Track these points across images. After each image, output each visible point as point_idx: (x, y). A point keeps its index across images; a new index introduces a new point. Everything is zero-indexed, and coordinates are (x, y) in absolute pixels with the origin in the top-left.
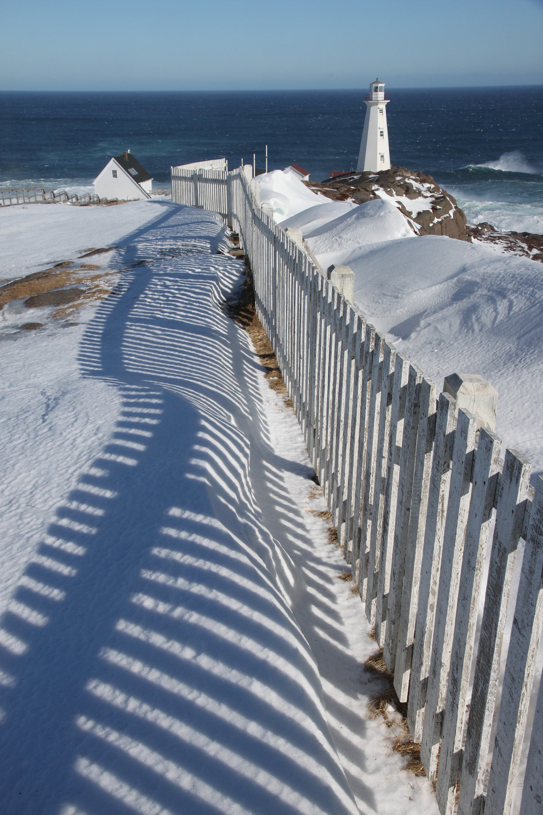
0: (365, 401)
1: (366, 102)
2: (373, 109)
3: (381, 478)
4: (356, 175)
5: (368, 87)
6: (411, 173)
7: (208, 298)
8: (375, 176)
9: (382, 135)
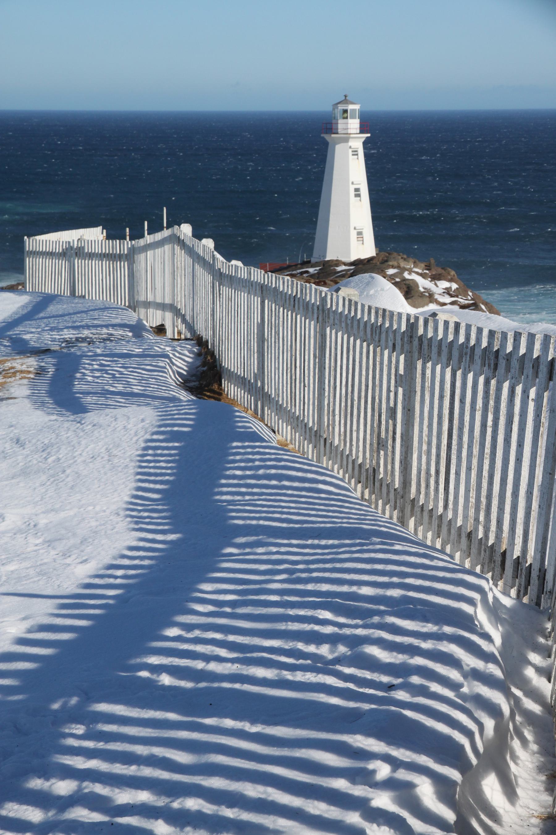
0: (376, 364)
2: (339, 149)
3: (390, 407)
4: (312, 267)
6: (415, 262)
8: (347, 268)
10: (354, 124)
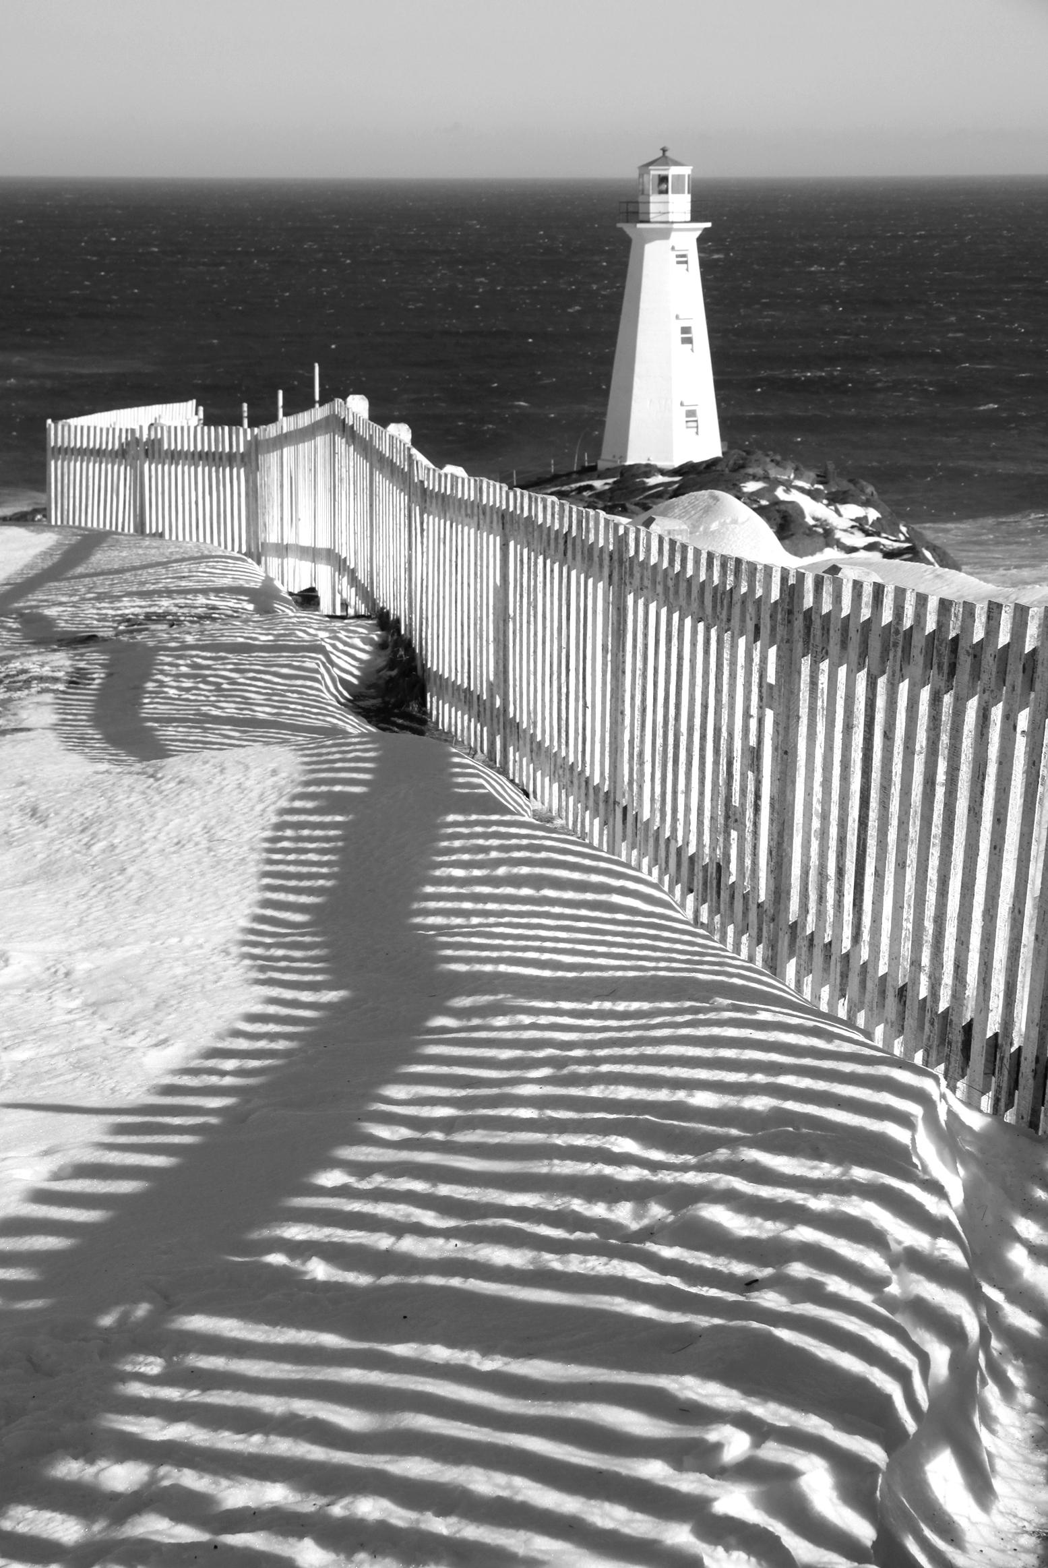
1: (627, 228)
4: (599, 477)
5: (633, 174)
6: (796, 470)
7: (316, 685)
9: (688, 341)
10: (679, 205)
